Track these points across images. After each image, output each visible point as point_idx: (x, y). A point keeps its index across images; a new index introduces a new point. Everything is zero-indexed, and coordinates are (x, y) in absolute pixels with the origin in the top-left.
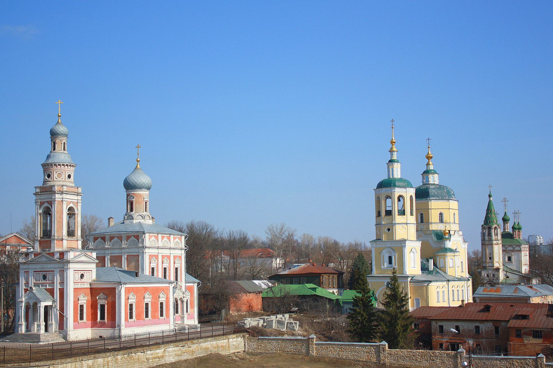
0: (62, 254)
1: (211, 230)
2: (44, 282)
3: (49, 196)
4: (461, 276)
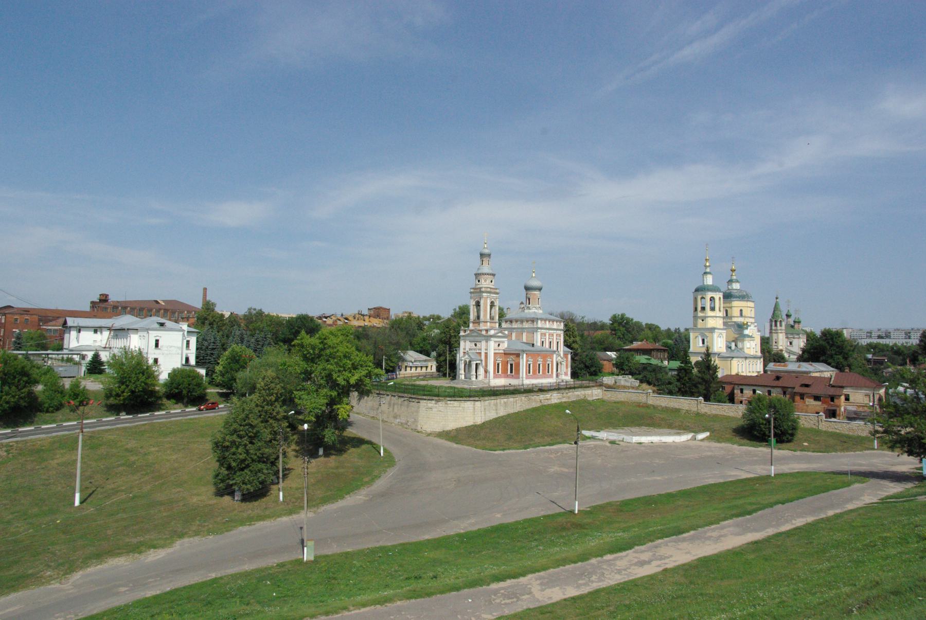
0: (487, 331)
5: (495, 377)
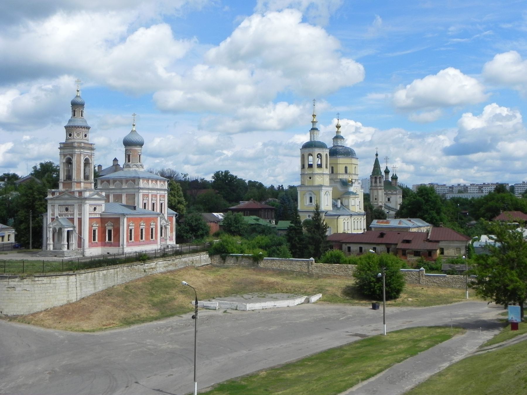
0: (80, 193)
1: (177, 175)
2: (66, 213)
3: (71, 150)
4: (360, 212)
5: (91, 245)
